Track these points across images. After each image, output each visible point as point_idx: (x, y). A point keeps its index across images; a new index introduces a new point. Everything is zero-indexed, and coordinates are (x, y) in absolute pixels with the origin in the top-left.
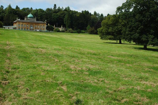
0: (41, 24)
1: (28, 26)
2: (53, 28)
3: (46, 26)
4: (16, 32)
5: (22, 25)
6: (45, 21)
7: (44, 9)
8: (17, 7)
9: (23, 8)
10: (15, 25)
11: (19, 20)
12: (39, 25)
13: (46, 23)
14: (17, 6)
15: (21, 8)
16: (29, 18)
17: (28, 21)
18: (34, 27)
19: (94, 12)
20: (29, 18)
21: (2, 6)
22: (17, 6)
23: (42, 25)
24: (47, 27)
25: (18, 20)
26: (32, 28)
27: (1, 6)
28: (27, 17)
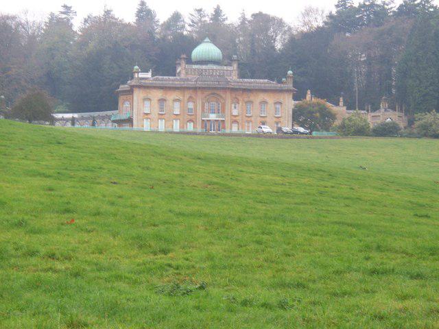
0: (262, 97)
1: (191, 105)
2: (333, 116)
3: (289, 103)
4: (326, 138)
5: (162, 101)
6: (285, 75)
7: (264, 13)
8: (145, 14)
9: (259, 17)
10: (127, 105)
11: (149, 75)
12: (252, 98)
13: (290, 86)
14: (218, 7)
15: (162, 16)
16: (198, 63)
17: (193, 79)
18: (223, 110)
19: (140, 11)
20: (198, 63)
21: (67, 9)
22: (218, 7)
23: (270, 99)
24: (294, 112)
25: (141, 75)
26: (213, 117)
27: (65, 6)
28: (189, 61)
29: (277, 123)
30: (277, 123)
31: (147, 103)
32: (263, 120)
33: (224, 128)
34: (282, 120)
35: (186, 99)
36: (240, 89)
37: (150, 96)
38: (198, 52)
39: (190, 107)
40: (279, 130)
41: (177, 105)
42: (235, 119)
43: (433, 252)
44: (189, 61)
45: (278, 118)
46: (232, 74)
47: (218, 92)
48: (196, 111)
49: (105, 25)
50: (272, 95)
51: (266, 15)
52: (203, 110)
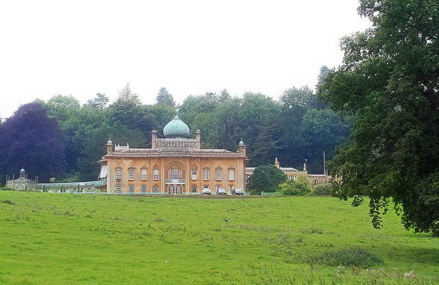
0: (217, 163)
1: (156, 172)
11: (127, 148)
13: (243, 154)
14: (163, 90)
18: (184, 177)
21: (164, 89)
23: (225, 166)
26: (175, 182)
28: (161, 135)
29: (231, 186)
30: (231, 186)
31: (231, 172)
32: (219, 183)
33: (184, 191)
34: (235, 183)
35: (152, 167)
36: (198, 158)
37: (121, 165)
38: (168, 128)
39: (195, 176)
40: (234, 192)
41: (144, 172)
42: (194, 183)
43: (3, 281)
44: (161, 135)
45: (206, 181)
46: (195, 147)
47: (178, 161)
48: (160, 178)
49: (294, 95)
50: (226, 162)
51: (20, 109)
52: (166, 177)
